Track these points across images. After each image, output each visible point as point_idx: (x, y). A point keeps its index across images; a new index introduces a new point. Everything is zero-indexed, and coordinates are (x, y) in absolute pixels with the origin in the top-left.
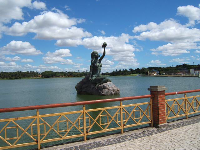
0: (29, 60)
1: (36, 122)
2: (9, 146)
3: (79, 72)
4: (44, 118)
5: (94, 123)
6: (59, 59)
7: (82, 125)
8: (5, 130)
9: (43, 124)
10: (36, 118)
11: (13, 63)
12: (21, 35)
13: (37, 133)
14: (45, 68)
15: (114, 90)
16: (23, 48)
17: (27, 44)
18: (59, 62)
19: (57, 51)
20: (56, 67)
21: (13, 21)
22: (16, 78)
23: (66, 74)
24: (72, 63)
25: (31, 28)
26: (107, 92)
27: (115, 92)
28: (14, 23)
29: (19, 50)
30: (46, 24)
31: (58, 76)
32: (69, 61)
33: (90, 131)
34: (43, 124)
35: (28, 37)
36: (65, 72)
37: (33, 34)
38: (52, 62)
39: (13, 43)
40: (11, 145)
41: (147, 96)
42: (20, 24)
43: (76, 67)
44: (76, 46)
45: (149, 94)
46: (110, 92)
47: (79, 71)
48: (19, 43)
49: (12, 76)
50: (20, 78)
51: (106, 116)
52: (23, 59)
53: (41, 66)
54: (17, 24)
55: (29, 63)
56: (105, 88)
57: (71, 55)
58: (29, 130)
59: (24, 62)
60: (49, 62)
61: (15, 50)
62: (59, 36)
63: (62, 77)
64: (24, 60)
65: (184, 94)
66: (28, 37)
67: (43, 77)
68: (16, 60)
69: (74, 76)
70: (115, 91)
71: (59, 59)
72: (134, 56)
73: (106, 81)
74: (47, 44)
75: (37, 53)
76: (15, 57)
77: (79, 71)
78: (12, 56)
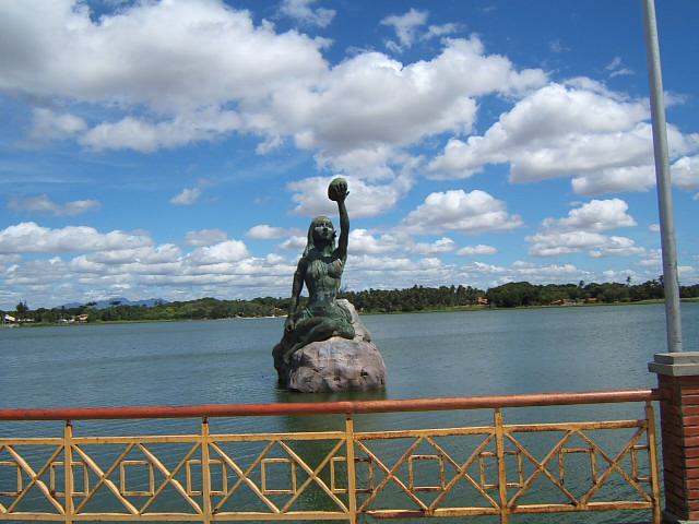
0: (482, 249)
1: (198, 454)
2: (129, 512)
3: (631, 285)
4: (221, 445)
5: (310, 480)
6: (583, 237)
7: (492, 475)
8: (263, 466)
9: (286, 460)
10: (199, 441)
11: (433, 261)
12: (467, 174)
13: (201, 489)
14: (533, 270)
15: (339, 374)
16: (469, 213)
17: (478, 198)
18: (585, 248)
19: (575, 212)
20: (570, 268)
21: (444, 138)
22: (406, 310)
23: (579, 293)
24: (634, 249)
25: (495, 150)
26: (305, 380)
27: (343, 381)
28: (445, 143)
29: (454, 218)
30: (542, 130)
31: (546, 302)
32: (623, 241)
33: (223, 509)
34: (286, 460)
35: (490, 177)
36: (577, 284)
37: (503, 169)
38: (558, 250)
39: (434, 199)
40: (278, 511)
41: (438, 401)
42: (463, 144)
43: (645, 262)
44: (646, 190)
45: (646, 385)
46: (319, 381)
47: (629, 279)
48: (455, 199)
49: (395, 303)
50: (419, 309)
51: (218, 464)
52: (465, 246)
53: (518, 267)
54: (454, 144)
55: (484, 257)
56: (305, 361)
57: (630, 222)
58: (324, 475)
59: (466, 256)
60: (547, 252)
61: (445, 218)
62: (583, 163)
63: (559, 304)
64: (468, 250)
65: (644, 403)
66: (490, 177)
67: (493, 304)
68: (445, 249)
69: (609, 300)
70: (345, 378)
71: (583, 237)
72: (635, 224)
73: (322, 334)
74: (546, 196)
75: (510, 225)
76: (439, 242)
77: (629, 279)
78: (432, 240)
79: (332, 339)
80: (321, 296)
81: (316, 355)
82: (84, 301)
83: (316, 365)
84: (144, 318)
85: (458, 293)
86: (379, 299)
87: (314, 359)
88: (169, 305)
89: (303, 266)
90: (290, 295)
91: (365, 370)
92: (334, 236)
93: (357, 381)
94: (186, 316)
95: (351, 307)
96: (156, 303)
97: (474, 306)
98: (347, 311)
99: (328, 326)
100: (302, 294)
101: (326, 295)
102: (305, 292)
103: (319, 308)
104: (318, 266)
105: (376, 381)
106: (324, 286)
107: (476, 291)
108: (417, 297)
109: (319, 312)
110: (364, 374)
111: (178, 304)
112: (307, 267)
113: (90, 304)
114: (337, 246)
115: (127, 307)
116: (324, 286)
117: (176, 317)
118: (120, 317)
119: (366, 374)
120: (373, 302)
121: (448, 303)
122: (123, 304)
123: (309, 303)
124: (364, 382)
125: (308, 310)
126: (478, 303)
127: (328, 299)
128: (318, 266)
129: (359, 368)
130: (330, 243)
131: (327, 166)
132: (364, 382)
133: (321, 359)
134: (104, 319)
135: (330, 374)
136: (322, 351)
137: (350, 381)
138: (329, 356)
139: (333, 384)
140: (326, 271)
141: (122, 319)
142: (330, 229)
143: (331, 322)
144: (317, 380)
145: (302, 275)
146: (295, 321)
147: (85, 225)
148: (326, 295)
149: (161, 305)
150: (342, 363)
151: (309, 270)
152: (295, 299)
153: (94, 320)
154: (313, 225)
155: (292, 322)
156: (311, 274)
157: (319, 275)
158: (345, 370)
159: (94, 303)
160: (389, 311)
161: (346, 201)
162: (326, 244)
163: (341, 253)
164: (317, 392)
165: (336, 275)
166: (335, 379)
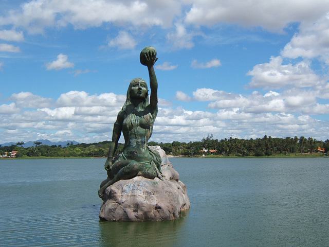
15: (137, 207)
22: (258, 155)
26: (110, 211)
27: (140, 213)
49: (249, 149)
50: (268, 154)
79: (136, 178)
80: (134, 143)
81: (120, 191)
82: (15, 140)
83: (120, 199)
84: (58, 155)
85: (300, 143)
86: (236, 146)
87: (118, 193)
88: (79, 145)
89: (121, 117)
90: (110, 140)
91: (159, 205)
92: (147, 94)
93: (153, 213)
94: (90, 155)
95: (161, 152)
96: (68, 144)
97: (314, 154)
98: (158, 156)
99: (133, 167)
100: (119, 142)
101: (137, 142)
102: (122, 140)
103: (132, 153)
104: (132, 119)
105: (168, 214)
106: (136, 135)
107: (316, 142)
108: (266, 145)
109: (132, 156)
110: (158, 208)
111: (84, 146)
112: (123, 120)
113: (19, 144)
114: (149, 103)
115: (46, 147)
116: (136, 135)
117: (82, 155)
118: (40, 154)
119: (160, 208)
120: (231, 148)
121: (292, 151)
122: (43, 144)
123: (124, 148)
124: (158, 214)
125: (124, 151)
126: (317, 151)
127: (139, 146)
128: (132, 119)
129: (155, 202)
130: (144, 100)
131: (314, 24)
132: (158, 214)
133: (124, 194)
134: (28, 155)
135: (130, 207)
136: (125, 188)
137: (145, 213)
138: (134, 192)
139: (132, 214)
140: (138, 123)
141: (42, 155)
142: (144, 89)
143: (135, 164)
144: (119, 211)
145: (120, 127)
146: (113, 162)
147: (104, 93)
148: (137, 142)
149: (71, 145)
150: (141, 198)
151: (125, 121)
152: (114, 144)
153: (21, 156)
154: (131, 85)
155: (110, 163)
156: (126, 125)
157: (132, 126)
158: (142, 203)
159: (22, 143)
160: (244, 155)
161: (157, 67)
162: (142, 101)
163: (153, 108)
164: (119, 221)
165: (147, 126)
166: (134, 211)
